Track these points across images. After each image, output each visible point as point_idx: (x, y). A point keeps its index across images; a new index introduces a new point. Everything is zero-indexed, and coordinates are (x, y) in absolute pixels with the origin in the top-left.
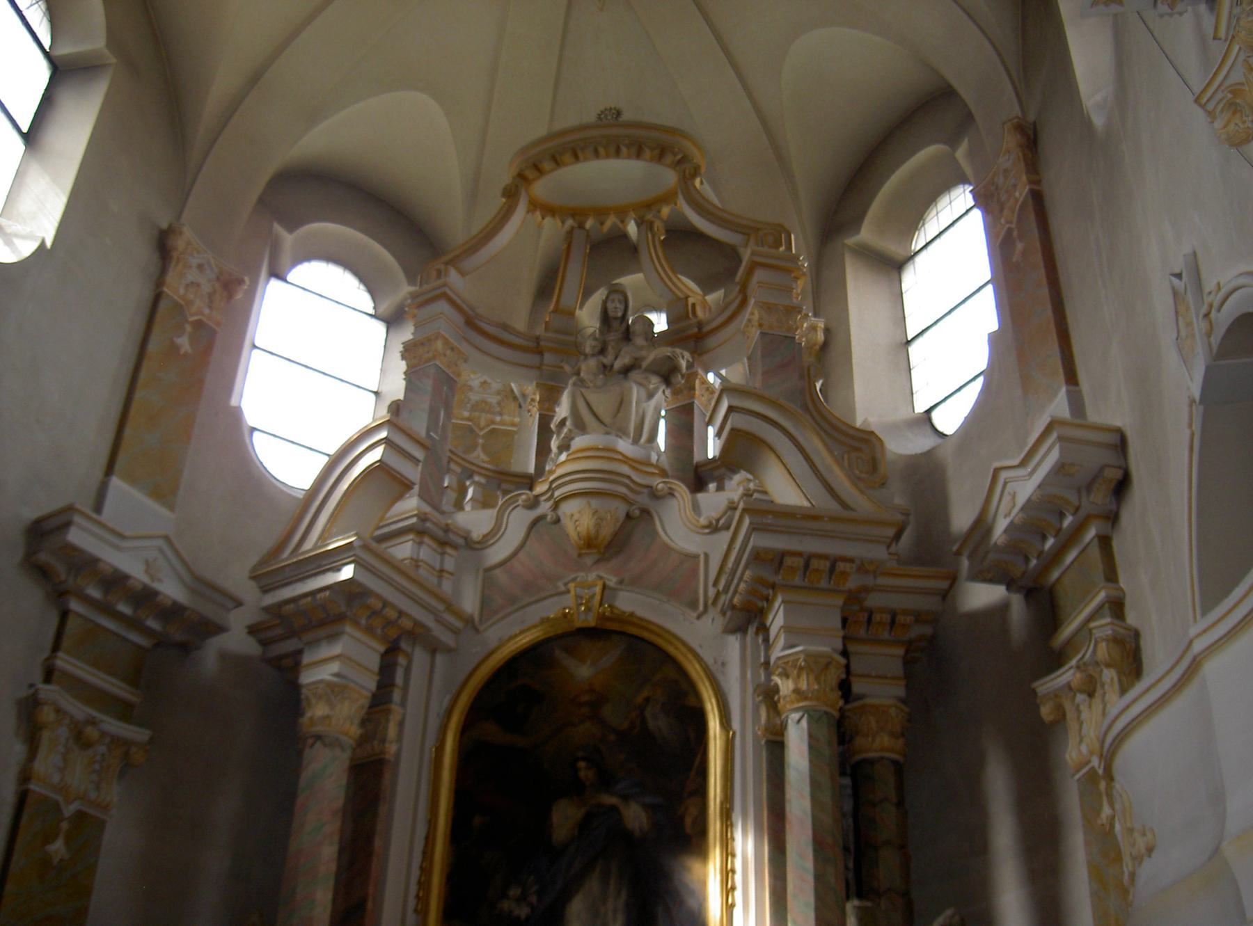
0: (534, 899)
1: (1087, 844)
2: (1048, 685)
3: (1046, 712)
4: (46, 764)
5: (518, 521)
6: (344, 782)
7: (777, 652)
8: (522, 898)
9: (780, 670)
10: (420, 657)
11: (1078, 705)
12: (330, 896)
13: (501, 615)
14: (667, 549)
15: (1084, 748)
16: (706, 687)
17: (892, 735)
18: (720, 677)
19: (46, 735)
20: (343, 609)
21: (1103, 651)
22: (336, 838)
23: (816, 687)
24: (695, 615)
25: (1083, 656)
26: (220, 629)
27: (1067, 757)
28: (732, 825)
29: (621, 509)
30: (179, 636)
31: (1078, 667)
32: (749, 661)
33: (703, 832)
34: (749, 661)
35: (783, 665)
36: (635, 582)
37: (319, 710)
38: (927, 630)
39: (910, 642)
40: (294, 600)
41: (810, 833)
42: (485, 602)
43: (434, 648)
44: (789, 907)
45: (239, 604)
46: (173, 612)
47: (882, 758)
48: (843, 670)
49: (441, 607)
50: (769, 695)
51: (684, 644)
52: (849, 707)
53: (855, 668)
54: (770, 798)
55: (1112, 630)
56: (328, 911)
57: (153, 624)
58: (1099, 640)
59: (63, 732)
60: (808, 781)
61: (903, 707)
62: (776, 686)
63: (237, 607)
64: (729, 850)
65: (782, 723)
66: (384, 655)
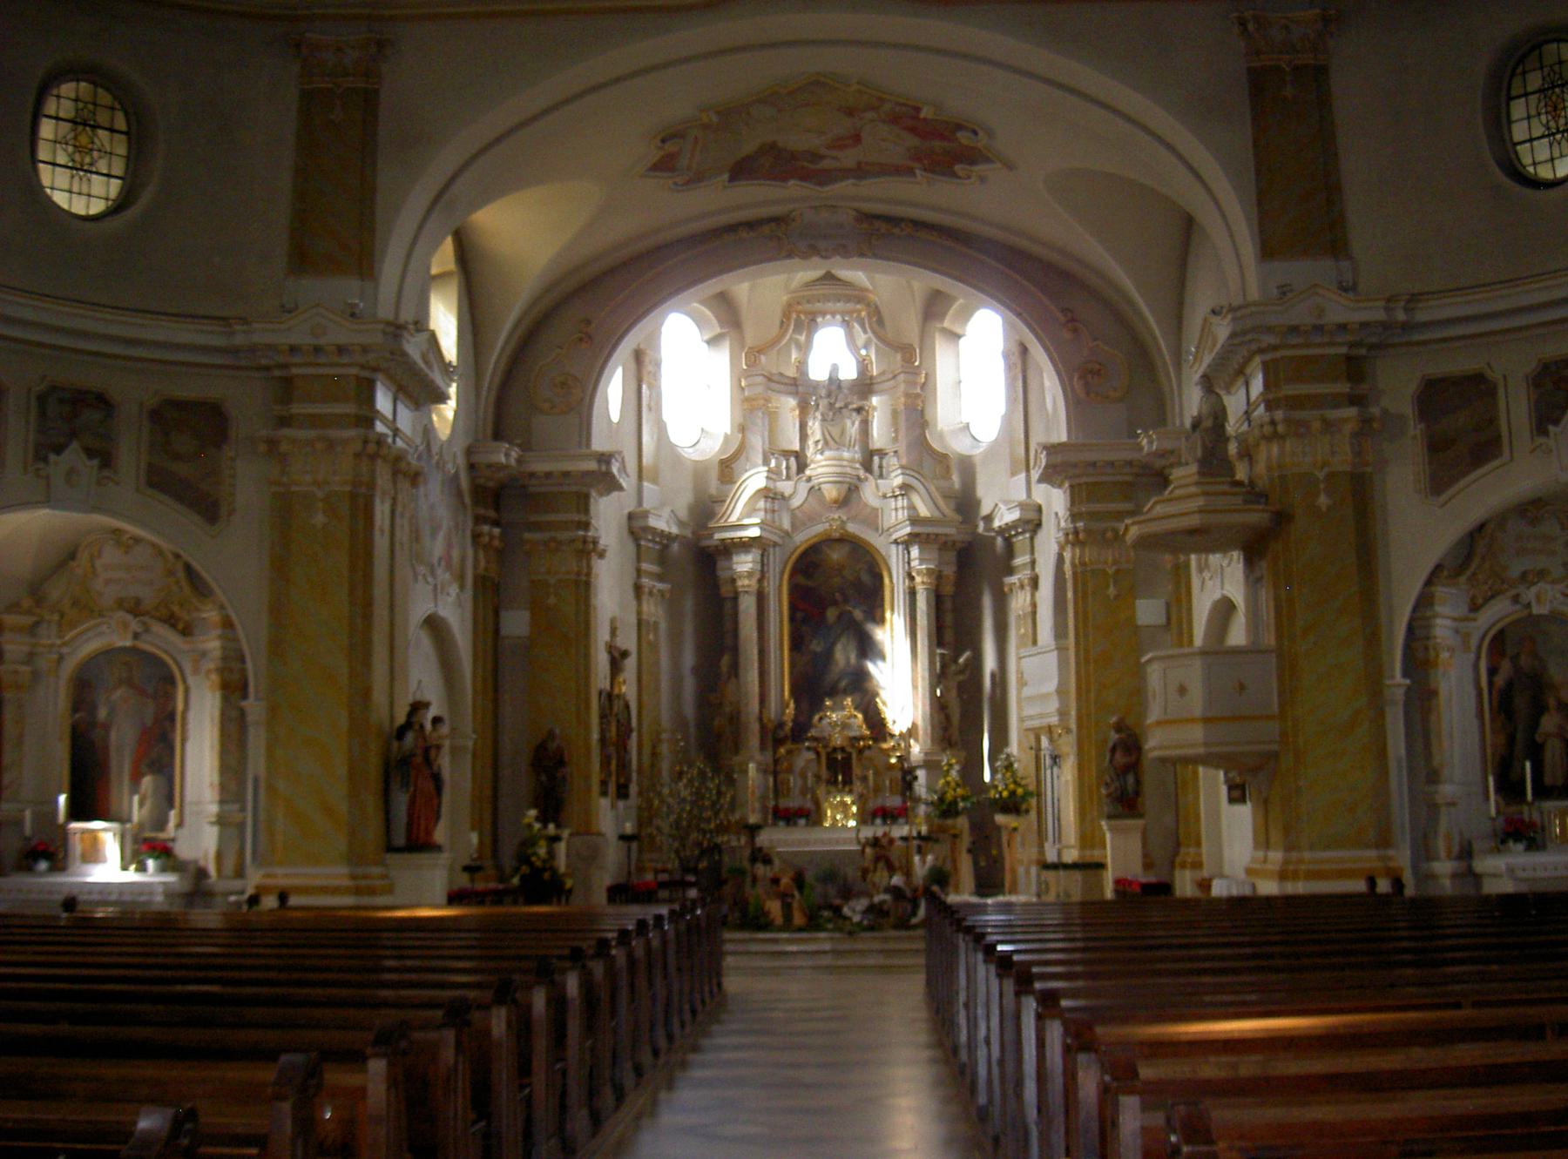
3: (1006, 589)
5: (803, 489)
14: (866, 505)
29: (846, 486)
36: (853, 519)
42: (793, 525)
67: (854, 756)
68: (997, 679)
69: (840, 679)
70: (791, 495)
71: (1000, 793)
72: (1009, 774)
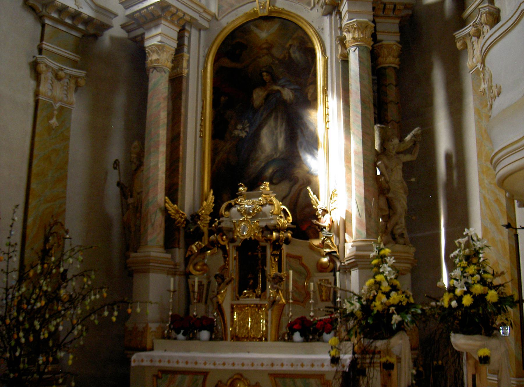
0: (247, 129)
1: (474, 99)
2: (460, 34)
3: (459, 45)
4: (44, 88)
6: (167, 86)
7: (345, 22)
8: (243, 129)
9: (346, 29)
10: (194, 33)
11: (473, 42)
12: (165, 132)
13: (226, 13)
15: (474, 60)
16: (315, 39)
17: (394, 57)
18: (321, 35)
19: (43, 77)
20: (160, 13)
21: (484, 18)
22: (166, 109)
23: (362, 36)
24: (310, 8)
25: (476, 20)
26: (108, 27)
27: (467, 64)
28: (327, 96)
30: (92, 31)
31: (473, 26)
32: (333, 26)
33: (315, 99)
34: (333, 26)
35: (347, 28)
37: (154, 57)
38: (410, 12)
39: (402, 17)
40: (139, 11)
41: (359, 97)
43: (200, 29)
44: (351, 127)
45: (116, 15)
46: (88, 21)
47: (389, 67)
48: (374, 29)
49: (201, 10)
50: (342, 41)
51: (306, 21)
52: (375, 45)
53: (378, 28)
54: (343, 83)
55: (489, 9)
56: (165, 138)
57: (80, 26)
58: (483, 13)
59: (50, 75)
60: (358, 76)
61: (399, 45)
62: (345, 36)
63: (115, 17)
64: (326, 106)
65: (347, 53)
66: (179, 33)
67: (269, 251)
68: (454, 160)
69: (265, 168)
70: (379, 199)
71: (459, 299)
72: (472, 269)
